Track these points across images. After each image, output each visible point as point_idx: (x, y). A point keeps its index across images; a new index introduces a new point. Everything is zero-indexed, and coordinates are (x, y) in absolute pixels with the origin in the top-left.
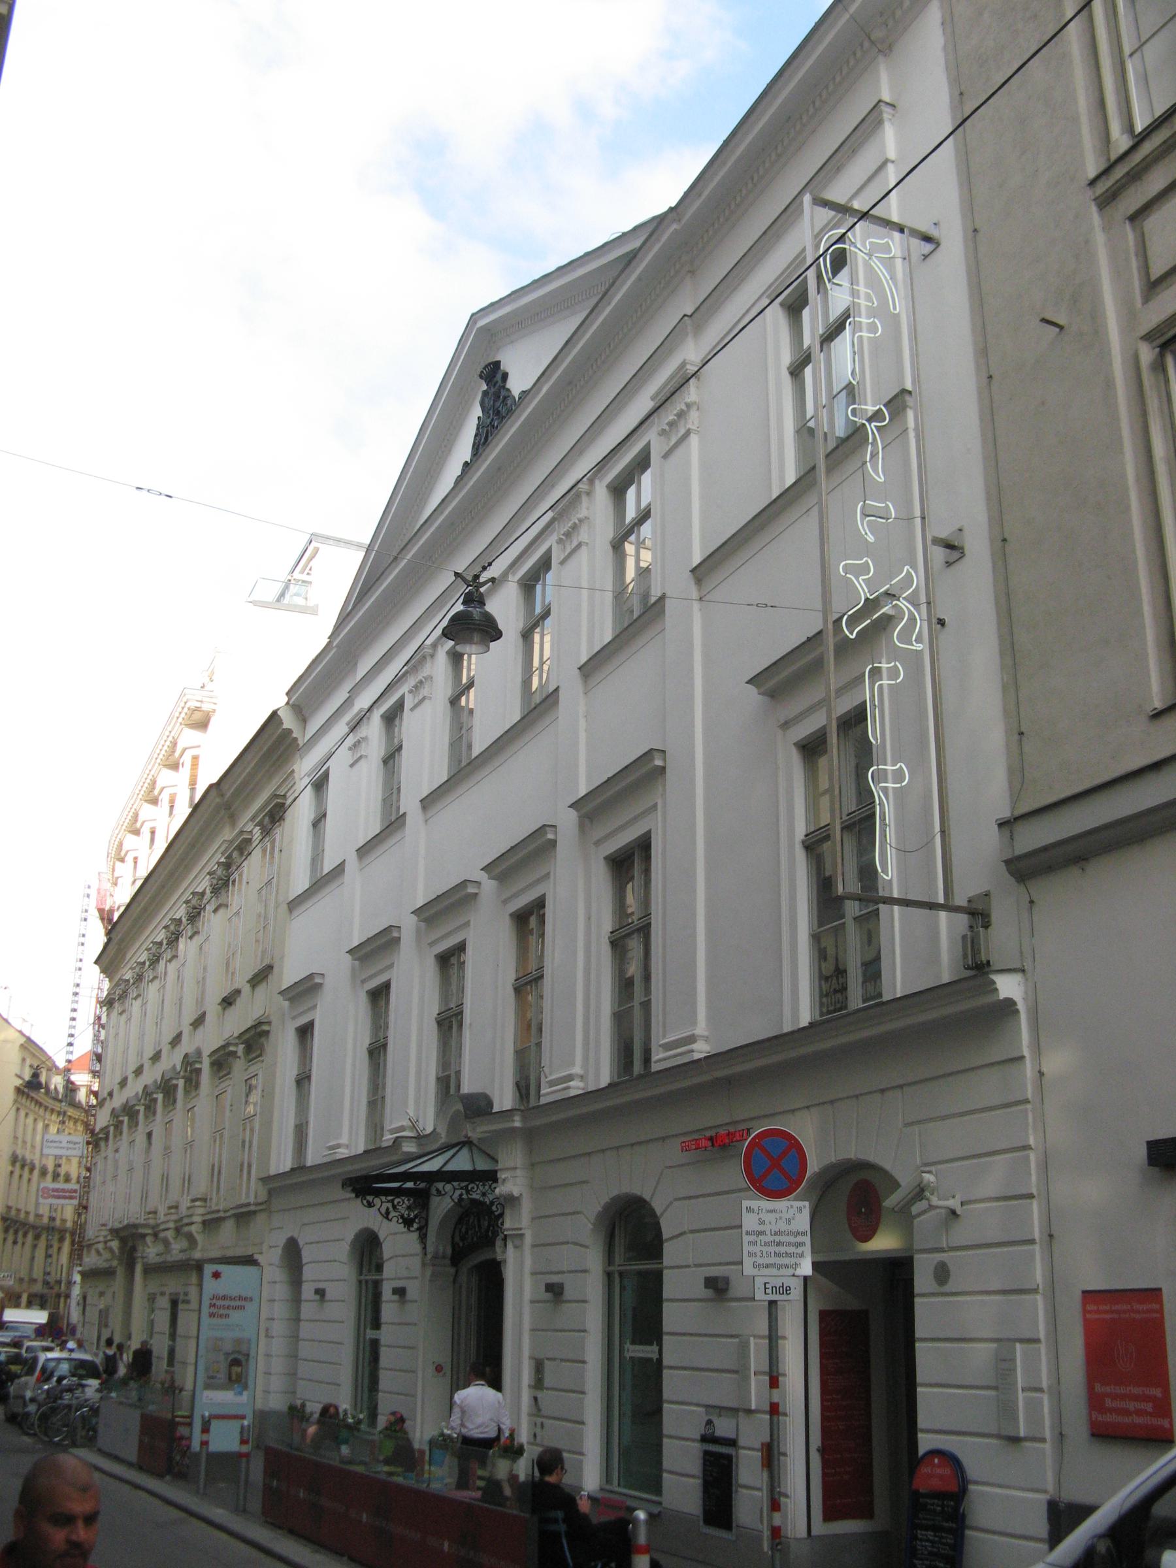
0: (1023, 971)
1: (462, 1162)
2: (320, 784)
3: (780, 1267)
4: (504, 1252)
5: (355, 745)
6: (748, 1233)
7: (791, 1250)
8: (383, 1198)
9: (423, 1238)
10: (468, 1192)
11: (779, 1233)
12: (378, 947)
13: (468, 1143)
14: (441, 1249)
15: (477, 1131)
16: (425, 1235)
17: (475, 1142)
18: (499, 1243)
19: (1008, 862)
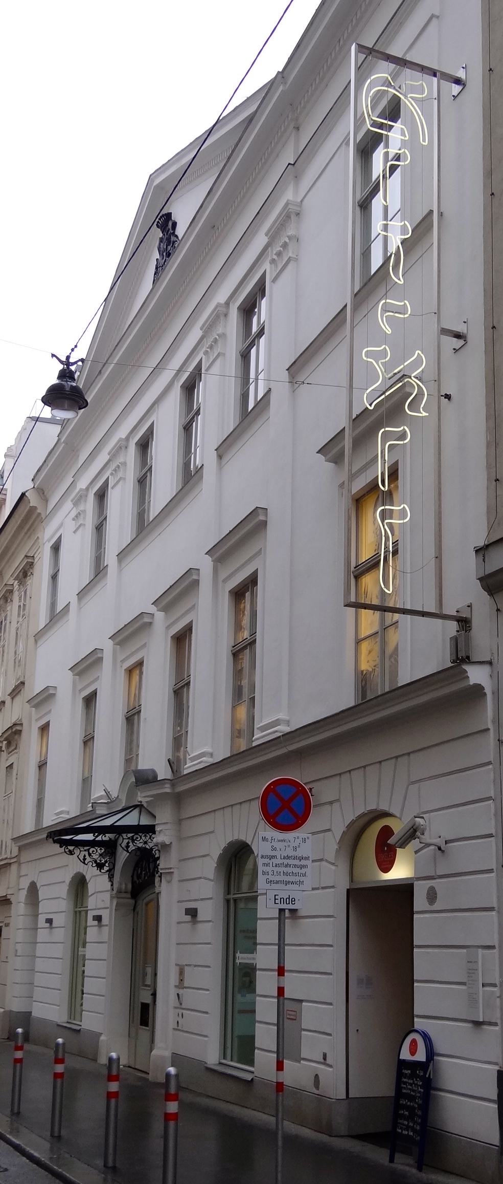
0: (490, 663)
1: (132, 819)
2: (56, 548)
3: (287, 883)
4: (160, 886)
5: (76, 516)
6: (262, 857)
7: (296, 870)
9: (111, 878)
11: (288, 857)
12: (88, 665)
13: (140, 806)
14: (124, 886)
15: (142, 797)
16: (113, 875)
17: (145, 805)
18: (157, 879)
19: (481, 579)
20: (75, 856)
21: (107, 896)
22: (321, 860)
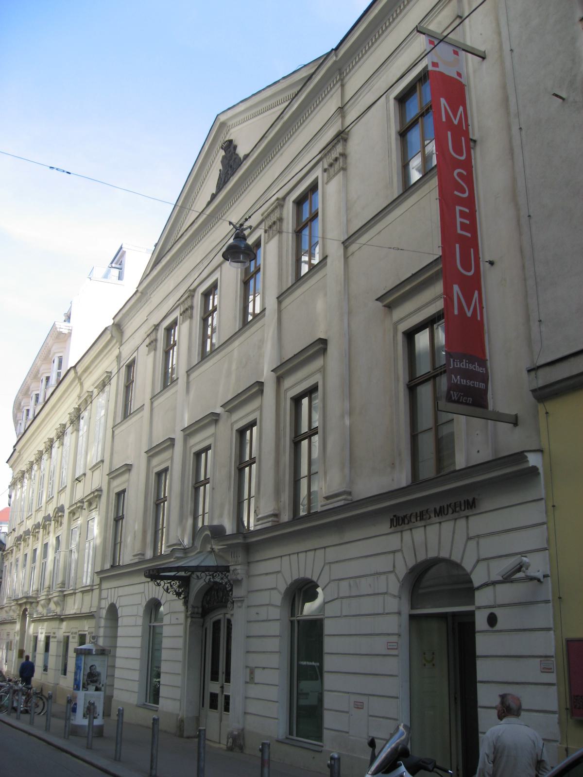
8: (166, 581)
9: (186, 603)
10: (213, 577)
16: (187, 601)
20: (161, 587)
21: (182, 617)
22: (386, 593)
